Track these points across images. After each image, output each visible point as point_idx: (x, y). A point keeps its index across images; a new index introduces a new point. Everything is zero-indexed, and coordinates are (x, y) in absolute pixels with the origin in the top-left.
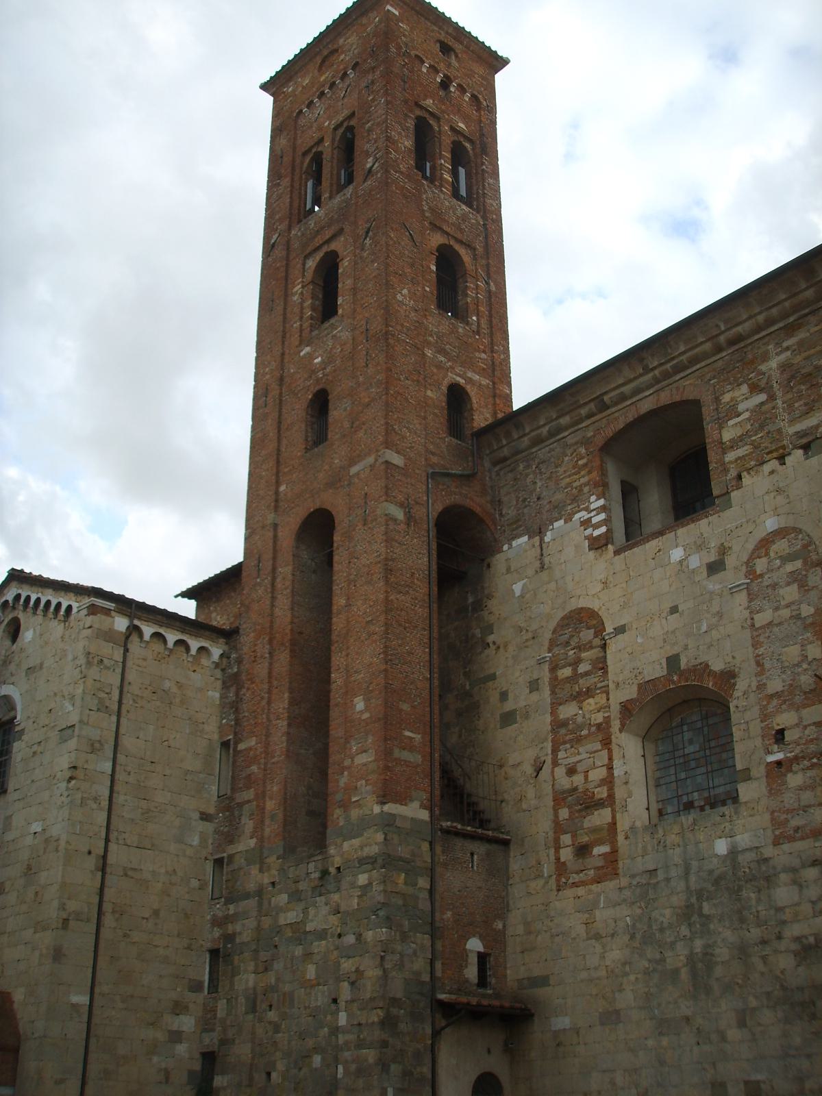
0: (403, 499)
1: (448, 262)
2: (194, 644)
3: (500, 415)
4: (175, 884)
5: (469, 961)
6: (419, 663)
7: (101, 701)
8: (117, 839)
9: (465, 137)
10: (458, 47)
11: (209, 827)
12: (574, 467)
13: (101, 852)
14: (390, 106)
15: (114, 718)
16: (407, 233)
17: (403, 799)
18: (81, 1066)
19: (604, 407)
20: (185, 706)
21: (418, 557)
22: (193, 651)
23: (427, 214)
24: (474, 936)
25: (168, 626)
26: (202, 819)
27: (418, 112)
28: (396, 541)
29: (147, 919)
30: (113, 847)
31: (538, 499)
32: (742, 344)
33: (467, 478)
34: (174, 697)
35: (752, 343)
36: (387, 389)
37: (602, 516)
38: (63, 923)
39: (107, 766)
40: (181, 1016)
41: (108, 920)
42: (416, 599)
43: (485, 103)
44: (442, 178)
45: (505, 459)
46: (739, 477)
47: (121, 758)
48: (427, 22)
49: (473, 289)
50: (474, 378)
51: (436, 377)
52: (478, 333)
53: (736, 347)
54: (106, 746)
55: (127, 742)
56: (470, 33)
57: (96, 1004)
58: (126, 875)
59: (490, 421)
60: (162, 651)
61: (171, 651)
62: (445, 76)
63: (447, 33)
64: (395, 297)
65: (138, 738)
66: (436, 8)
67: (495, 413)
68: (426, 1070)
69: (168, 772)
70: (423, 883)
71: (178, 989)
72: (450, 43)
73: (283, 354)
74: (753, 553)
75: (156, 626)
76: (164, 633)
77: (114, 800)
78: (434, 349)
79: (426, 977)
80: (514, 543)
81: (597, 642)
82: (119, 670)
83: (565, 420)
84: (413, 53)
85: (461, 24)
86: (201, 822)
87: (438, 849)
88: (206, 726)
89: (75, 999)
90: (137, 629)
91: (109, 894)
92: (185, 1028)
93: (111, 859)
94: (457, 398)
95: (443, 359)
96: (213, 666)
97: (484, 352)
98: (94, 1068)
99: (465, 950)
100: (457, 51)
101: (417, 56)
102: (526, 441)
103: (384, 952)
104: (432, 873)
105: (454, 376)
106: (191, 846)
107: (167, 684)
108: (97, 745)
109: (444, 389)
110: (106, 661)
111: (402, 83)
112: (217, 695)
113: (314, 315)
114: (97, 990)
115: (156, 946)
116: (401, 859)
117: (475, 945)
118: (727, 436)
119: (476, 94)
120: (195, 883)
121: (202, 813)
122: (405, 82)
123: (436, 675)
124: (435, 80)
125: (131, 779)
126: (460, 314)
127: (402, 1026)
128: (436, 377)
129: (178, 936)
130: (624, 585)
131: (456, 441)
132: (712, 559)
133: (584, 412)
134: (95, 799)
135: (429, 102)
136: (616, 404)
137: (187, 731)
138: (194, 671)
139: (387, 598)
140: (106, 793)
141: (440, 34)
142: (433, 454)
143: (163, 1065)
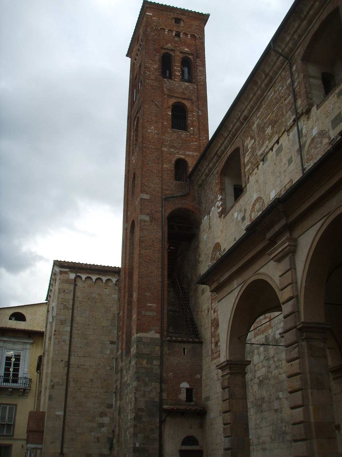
0: (149, 212)
2: (104, 279)
4: (99, 369)
5: (182, 392)
6: (156, 276)
7: (65, 305)
8: (74, 355)
9: (188, 54)
10: (183, 17)
11: (114, 346)
13: (67, 360)
14: (146, 54)
15: (71, 311)
16: (154, 104)
17: (146, 331)
18: (61, 437)
20: (102, 302)
22: (104, 281)
24: (184, 382)
25: (93, 273)
26: (111, 344)
27: (164, 51)
28: (145, 229)
29: (88, 383)
30: (72, 358)
33: (186, 196)
34: (97, 300)
38: (52, 387)
39: (68, 329)
40: (103, 417)
41: (72, 384)
42: (155, 250)
43: (198, 36)
44: (175, 75)
46: (248, 178)
47: (75, 325)
48: (167, 13)
49: (192, 116)
50: (189, 154)
51: (169, 158)
52: (193, 135)
54: (67, 321)
55: (77, 319)
56: (187, 10)
57: (67, 414)
58: (78, 367)
60: (92, 283)
62: (176, 32)
63: (177, 13)
64: (147, 131)
65: (82, 317)
66: (169, 6)
68: (156, 435)
69: (95, 328)
70: (156, 362)
71: (102, 408)
72: (180, 17)
74: (251, 211)
75: (88, 274)
77: (72, 341)
78: (168, 147)
79: (157, 400)
80: (205, 219)
82: (72, 293)
84: (159, 28)
85: (182, 8)
86: (110, 345)
87: (166, 348)
88: (112, 309)
89: (58, 413)
90: (80, 277)
91: (71, 375)
92: (105, 422)
93: (72, 362)
95: (173, 150)
96: (114, 285)
97: (196, 141)
98: (67, 436)
99: (180, 388)
100: (183, 19)
101: (161, 29)
102: (204, 176)
103: (136, 391)
104: (161, 358)
105: (179, 156)
106: (106, 354)
107: (94, 295)
108: (64, 322)
109: (173, 162)
110: (66, 291)
111: (153, 43)
112: (116, 296)
114: (67, 410)
115: (92, 392)
116: (145, 354)
117: (185, 385)
119: (193, 34)
120: (108, 368)
121: (110, 341)
122: (154, 41)
123: (166, 279)
124: (172, 35)
125: (79, 332)
126: (185, 128)
127: (144, 419)
128: (169, 158)
129: (102, 388)
131: (179, 182)
134: (64, 341)
137: (103, 311)
138: (106, 289)
140: (68, 338)
141: (174, 15)
142: (166, 190)
143: (96, 436)
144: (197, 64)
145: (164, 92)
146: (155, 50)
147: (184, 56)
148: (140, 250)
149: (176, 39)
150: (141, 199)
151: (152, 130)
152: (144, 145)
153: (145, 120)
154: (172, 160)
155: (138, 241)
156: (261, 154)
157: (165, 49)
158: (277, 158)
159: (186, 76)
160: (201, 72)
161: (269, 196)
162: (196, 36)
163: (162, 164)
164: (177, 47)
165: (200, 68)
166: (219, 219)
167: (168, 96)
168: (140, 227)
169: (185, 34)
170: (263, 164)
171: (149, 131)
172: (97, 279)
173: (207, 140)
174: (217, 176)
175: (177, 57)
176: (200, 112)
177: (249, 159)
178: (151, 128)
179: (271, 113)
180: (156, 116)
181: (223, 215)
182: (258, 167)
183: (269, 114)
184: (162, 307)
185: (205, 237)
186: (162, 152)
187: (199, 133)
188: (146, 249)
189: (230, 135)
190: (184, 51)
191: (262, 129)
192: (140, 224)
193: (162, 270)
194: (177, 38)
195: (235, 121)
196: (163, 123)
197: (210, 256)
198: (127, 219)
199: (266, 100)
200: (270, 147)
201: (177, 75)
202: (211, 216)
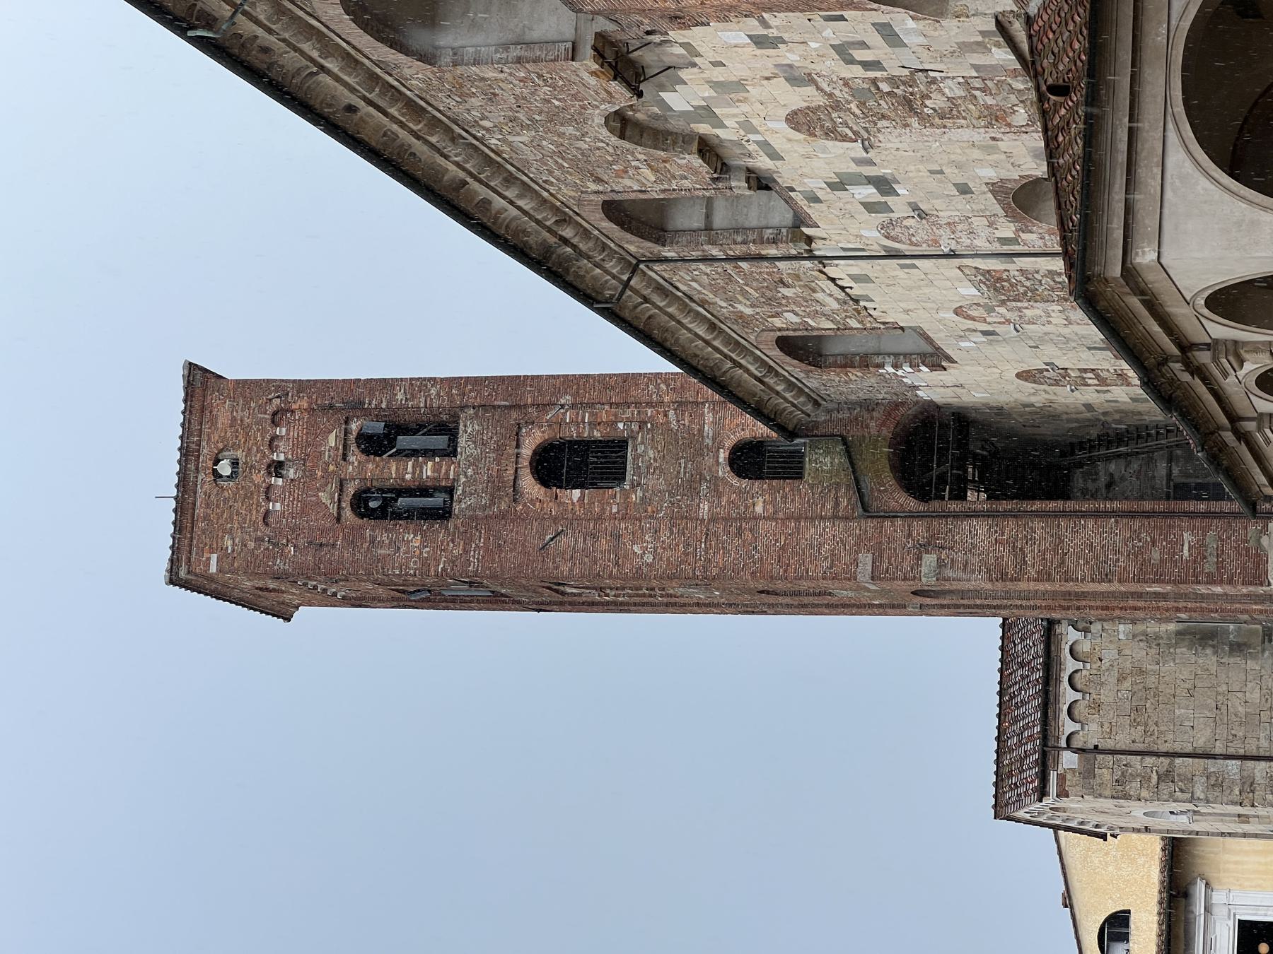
2: (1070, 665)
15: (1178, 761)
23: (503, 506)
27: (348, 513)
39: (1233, 765)
55: (1201, 740)
62: (270, 474)
64: (650, 565)
140: (1263, 764)
142: (837, 504)
144: (384, 406)
146: (352, 543)
147: (353, 447)
149: (291, 473)
150: (873, 578)
151: (642, 551)
157: (339, 508)
163: (756, 518)
164: (325, 470)
171: (649, 558)
175: (364, 469)
176: (562, 401)
180: (595, 537)
184: (1192, 515)
186: (714, 520)
187: (638, 404)
188: (1025, 563)
190: (338, 449)
198: (893, 607)
201: (436, 469)
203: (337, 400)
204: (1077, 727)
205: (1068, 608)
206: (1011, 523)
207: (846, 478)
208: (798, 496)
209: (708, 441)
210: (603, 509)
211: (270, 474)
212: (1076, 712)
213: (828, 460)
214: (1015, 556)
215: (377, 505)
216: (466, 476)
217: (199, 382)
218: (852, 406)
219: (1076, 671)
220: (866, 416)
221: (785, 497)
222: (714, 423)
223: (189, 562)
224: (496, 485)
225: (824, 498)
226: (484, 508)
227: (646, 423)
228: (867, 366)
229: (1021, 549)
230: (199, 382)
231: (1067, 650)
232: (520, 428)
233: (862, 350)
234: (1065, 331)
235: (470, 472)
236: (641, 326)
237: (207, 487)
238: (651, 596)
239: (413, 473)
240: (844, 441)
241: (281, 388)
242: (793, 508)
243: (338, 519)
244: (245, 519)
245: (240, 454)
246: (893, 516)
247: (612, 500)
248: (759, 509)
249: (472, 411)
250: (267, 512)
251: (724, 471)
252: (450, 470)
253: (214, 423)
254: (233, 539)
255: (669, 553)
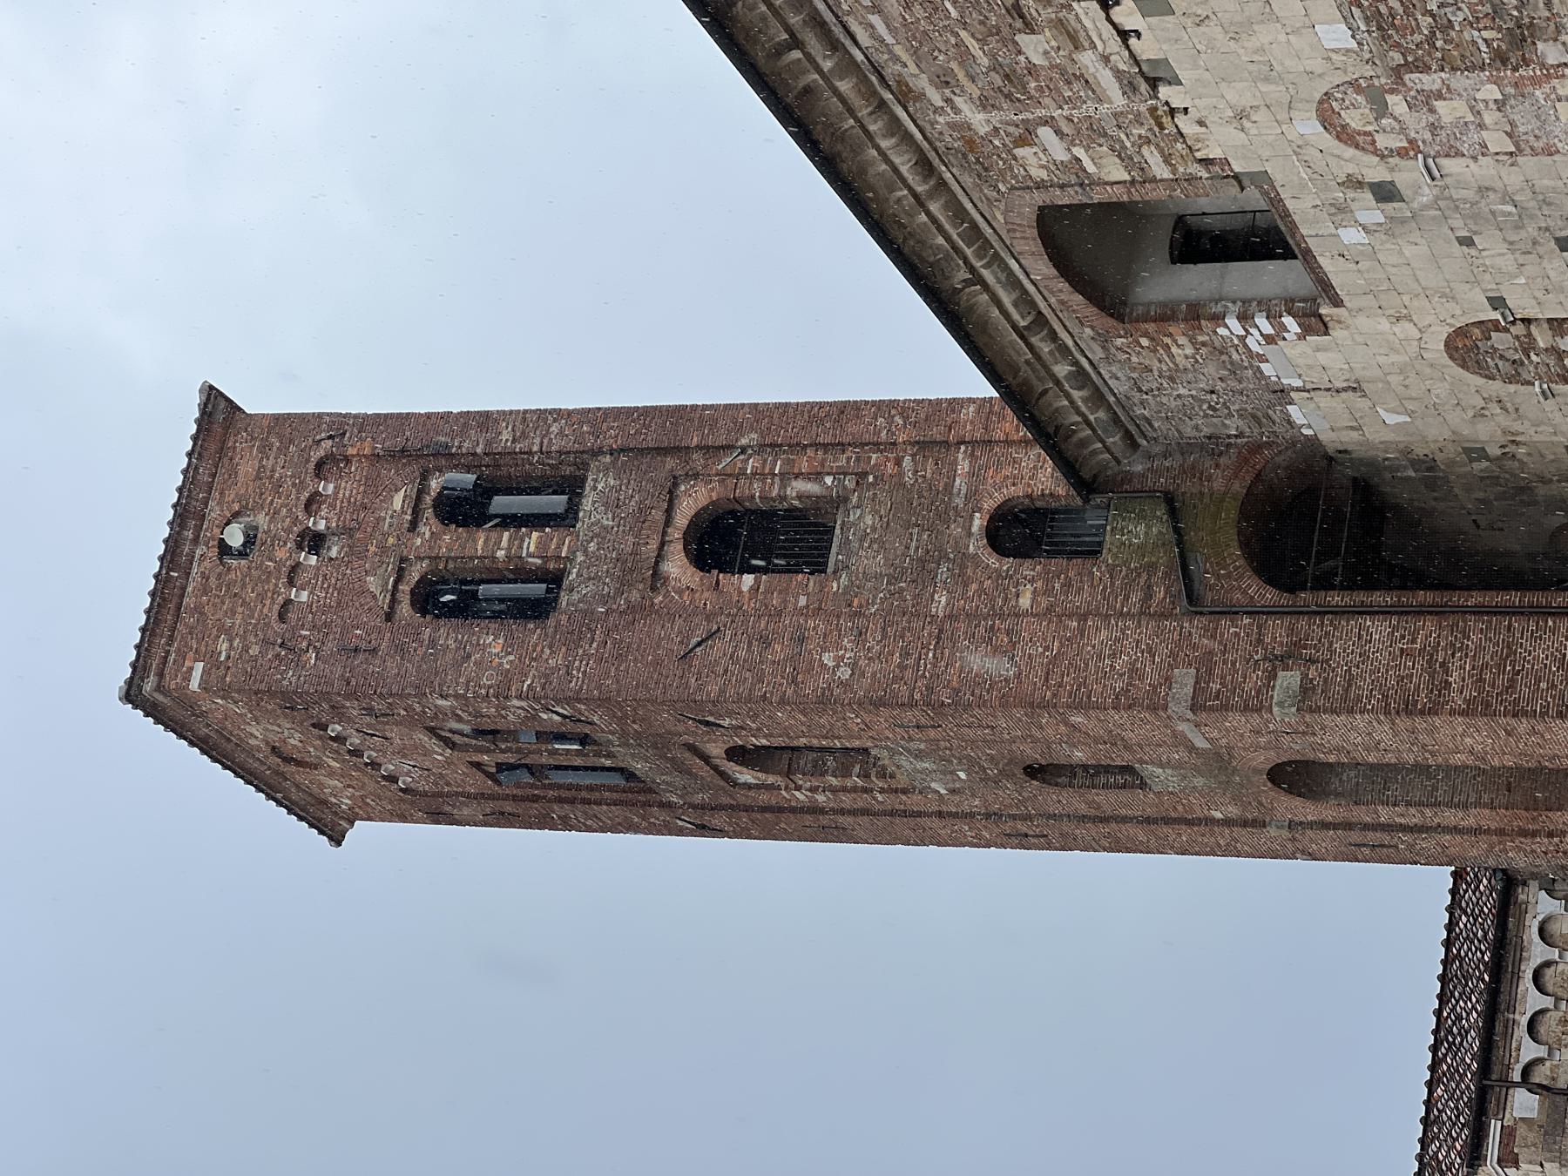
1: (721, 541)
2: (1537, 952)
3: (1024, 432)
12: (1155, 351)
19: (1040, 321)
21: (1372, 640)
23: (635, 596)
27: (405, 609)
31: (1212, 392)
32: (932, 155)
35: (930, 143)
36: (1045, 706)
37: (1262, 322)
45: (1128, 435)
46: (1206, 162)
53: (936, 162)
59: (1038, 450)
61: (1558, 999)
62: (300, 547)
64: (844, 685)
67: (1027, 442)
73: (940, 814)
76: (1528, 1015)
81: (1519, 329)
83: (1062, 370)
94: (1020, 531)
101: (282, 617)
113: (857, 768)
118: (1116, 172)
119: (312, 466)
130: (1406, 298)
132: (1370, 196)
133: (1045, 348)
135: (373, 583)
136: (1033, 304)
139: (1463, 713)
142: (1148, 596)
145: (632, 608)
147: (429, 513)
148: (1452, 712)
152: (917, 696)
153: (789, 692)
154: (996, 570)
155: (1403, 723)
156: (1124, 93)
157: (394, 601)
158: (1178, 13)
159: (557, 502)
160: (523, 433)
161: (1334, 56)
162: (322, 453)
165: (506, 436)
166: (1337, 333)
167: (653, 588)
168: (1334, 711)
169: (314, 507)
170: (1175, 81)
171: (844, 673)
172: (1540, 988)
173: (893, 412)
174: (1119, 342)
176: (744, 441)
177: (1119, 156)
178: (831, 664)
179: (963, 34)
180: (766, 642)
181: (1322, 311)
182: (1172, 112)
183: (960, 44)
185: (1392, 419)
189: (969, 252)
191: (1012, 83)
192: (1317, 710)
193: (1550, 614)
194: (329, 548)
195: (923, 217)
196: (800, 612)
197: (1496, 387)
199: (886, 57)
200: (1114, 44)
202: (1298, 383)
203: (409, 443)
204: (1542, 1052)
205: (1534, 834)
206: (1430, 623)
207: (1165, 558)
208: (1085, 584)
209: (959, 501)
210: (785, 601)
211: (300, 547)
212: (1542, 1030)
213: (1141, 528)
214: (1432, 676)
215: (447, 597)
216: (585, 551)
217: (217, 413)
218: (1186, 448)
219: (1548, 964)
220: (1208, 462)
221: (1067, 585)
222: (971, 474)
223: (161, 675)
224: (626, 570)
225: (1128, 587)
226: (604, 600)
227: (866, 474)
228: (1198, 318)
229: (1443, 665)
230: (217, 413)
231: (1535, 929)
232: (675, 485)
233: (1193, 295)
234: (1512, 178)
235: (592, 546)
236: (790, 99)
237: (207, 564)
238: (865, 790)
239: (509, 549)
240: (1169, 499)
241: (339, 426)
242: (1078, 601)
243: (389, 617)
244: (252, 611)
245: (262, 520)
246: (1232, 613)
247: (802, 590)
248: (1025, 602)
249: (608, 459)
250: (288, 602)
251: (977, 546)
252: (562, 543)
253: (233, 472)
254: (231, 641)
255: (876, 666)
